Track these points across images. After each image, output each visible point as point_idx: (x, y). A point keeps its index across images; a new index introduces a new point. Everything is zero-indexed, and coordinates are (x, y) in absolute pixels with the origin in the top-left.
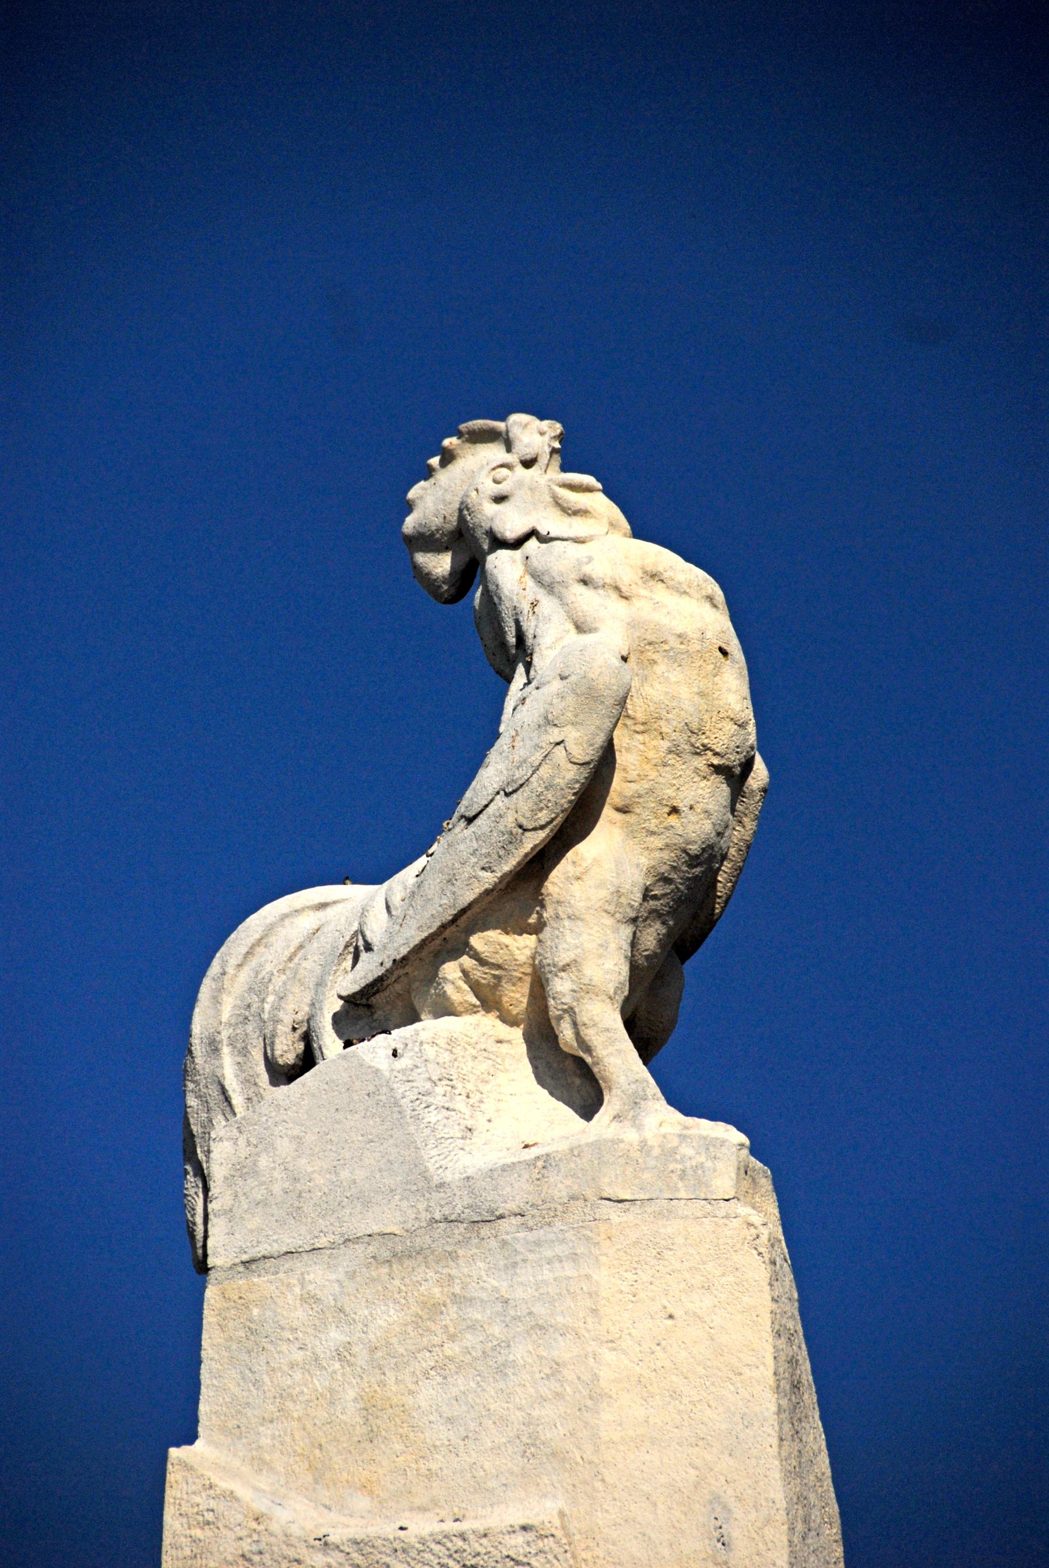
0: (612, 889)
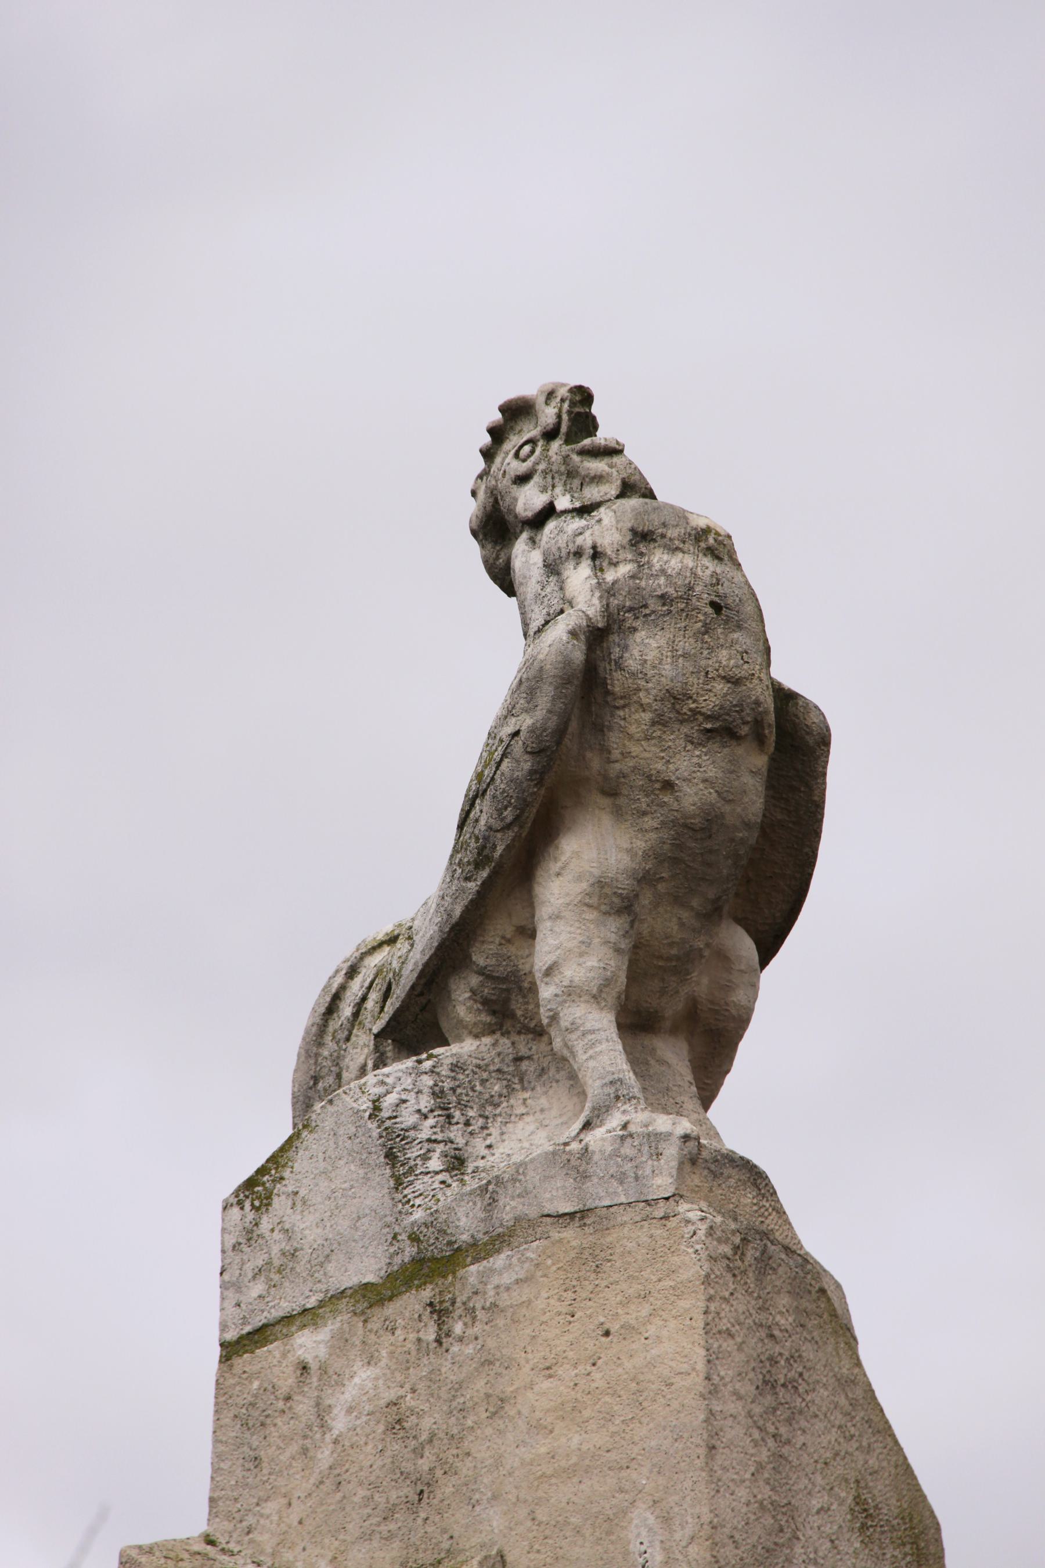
0: (592, 881)
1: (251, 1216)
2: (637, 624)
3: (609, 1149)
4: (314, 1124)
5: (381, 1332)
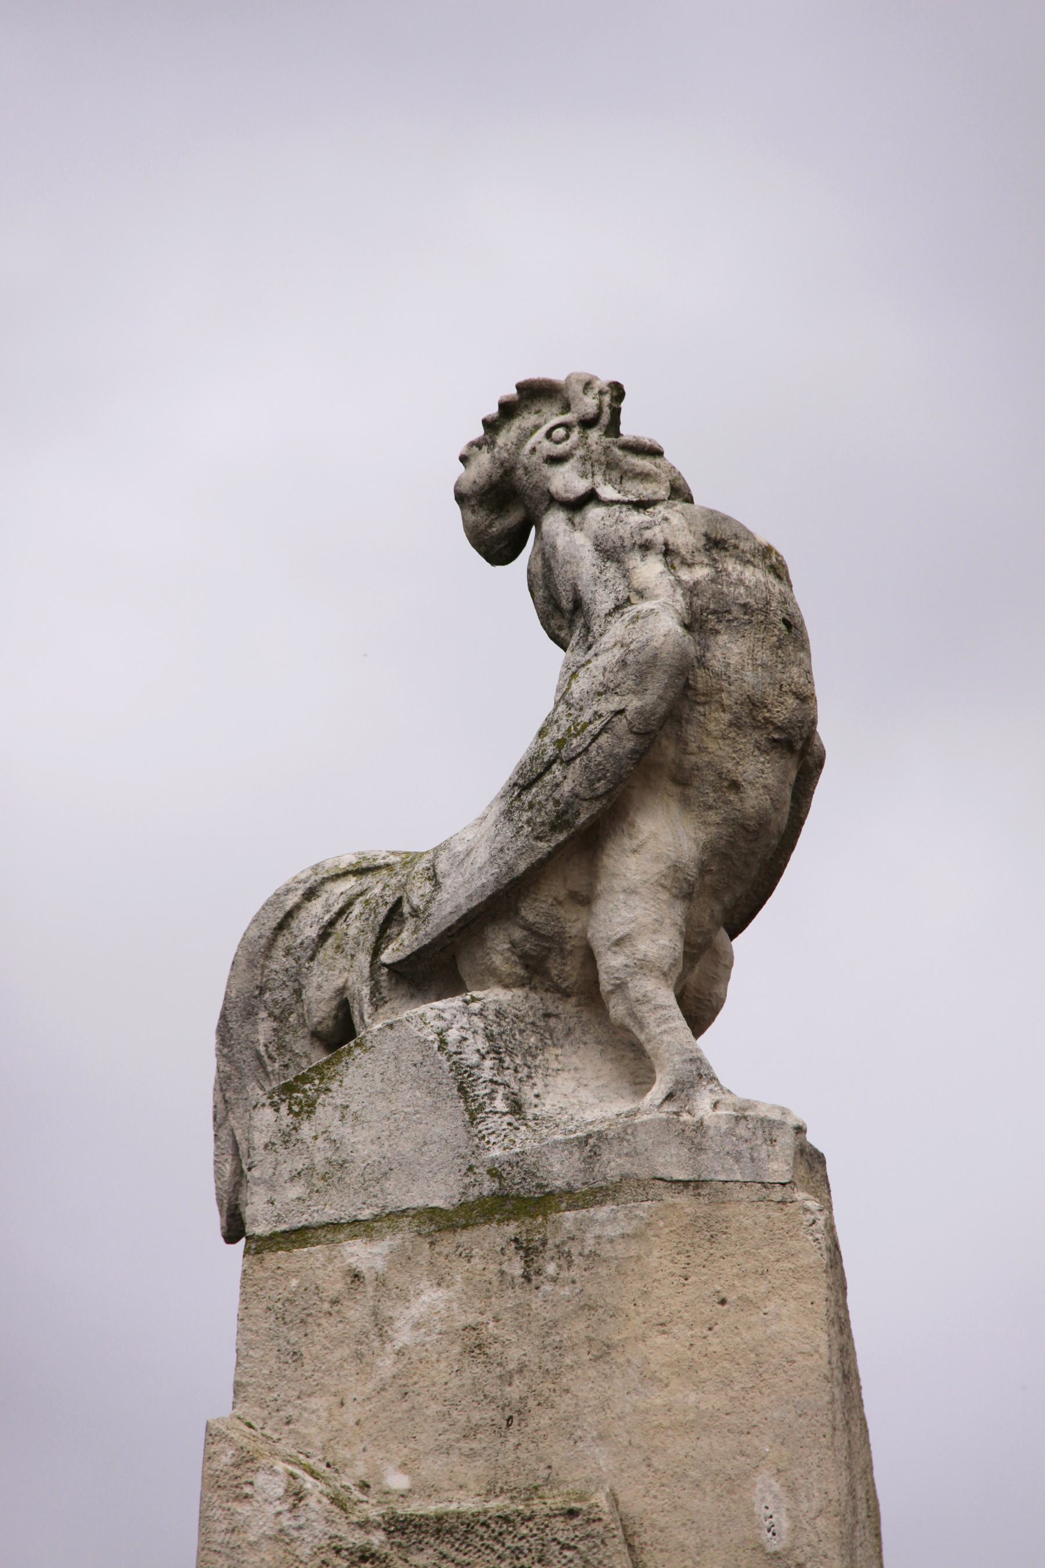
0: (669, 863)
1: (288, 1120)
2: (720, 627)
3: (724, 1127)
4: (369, 1044)
5: (453, 1257)
